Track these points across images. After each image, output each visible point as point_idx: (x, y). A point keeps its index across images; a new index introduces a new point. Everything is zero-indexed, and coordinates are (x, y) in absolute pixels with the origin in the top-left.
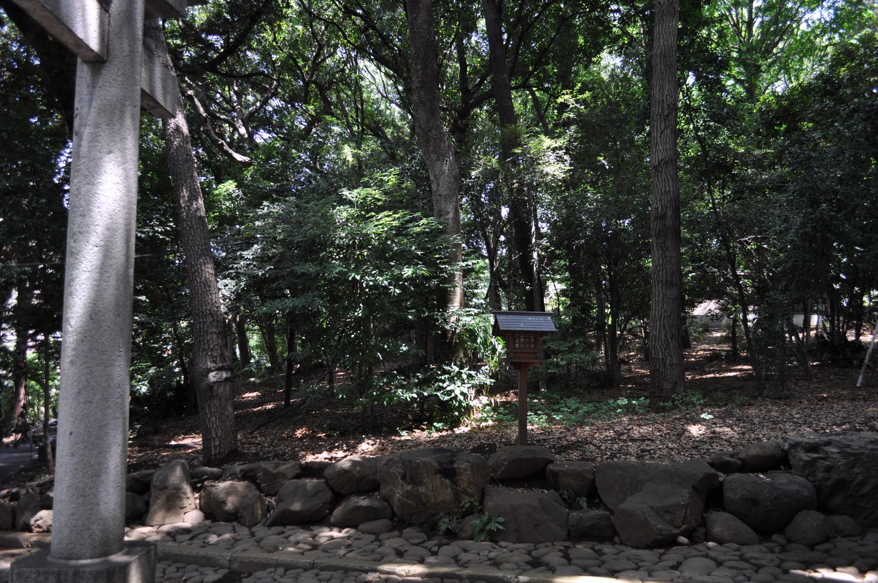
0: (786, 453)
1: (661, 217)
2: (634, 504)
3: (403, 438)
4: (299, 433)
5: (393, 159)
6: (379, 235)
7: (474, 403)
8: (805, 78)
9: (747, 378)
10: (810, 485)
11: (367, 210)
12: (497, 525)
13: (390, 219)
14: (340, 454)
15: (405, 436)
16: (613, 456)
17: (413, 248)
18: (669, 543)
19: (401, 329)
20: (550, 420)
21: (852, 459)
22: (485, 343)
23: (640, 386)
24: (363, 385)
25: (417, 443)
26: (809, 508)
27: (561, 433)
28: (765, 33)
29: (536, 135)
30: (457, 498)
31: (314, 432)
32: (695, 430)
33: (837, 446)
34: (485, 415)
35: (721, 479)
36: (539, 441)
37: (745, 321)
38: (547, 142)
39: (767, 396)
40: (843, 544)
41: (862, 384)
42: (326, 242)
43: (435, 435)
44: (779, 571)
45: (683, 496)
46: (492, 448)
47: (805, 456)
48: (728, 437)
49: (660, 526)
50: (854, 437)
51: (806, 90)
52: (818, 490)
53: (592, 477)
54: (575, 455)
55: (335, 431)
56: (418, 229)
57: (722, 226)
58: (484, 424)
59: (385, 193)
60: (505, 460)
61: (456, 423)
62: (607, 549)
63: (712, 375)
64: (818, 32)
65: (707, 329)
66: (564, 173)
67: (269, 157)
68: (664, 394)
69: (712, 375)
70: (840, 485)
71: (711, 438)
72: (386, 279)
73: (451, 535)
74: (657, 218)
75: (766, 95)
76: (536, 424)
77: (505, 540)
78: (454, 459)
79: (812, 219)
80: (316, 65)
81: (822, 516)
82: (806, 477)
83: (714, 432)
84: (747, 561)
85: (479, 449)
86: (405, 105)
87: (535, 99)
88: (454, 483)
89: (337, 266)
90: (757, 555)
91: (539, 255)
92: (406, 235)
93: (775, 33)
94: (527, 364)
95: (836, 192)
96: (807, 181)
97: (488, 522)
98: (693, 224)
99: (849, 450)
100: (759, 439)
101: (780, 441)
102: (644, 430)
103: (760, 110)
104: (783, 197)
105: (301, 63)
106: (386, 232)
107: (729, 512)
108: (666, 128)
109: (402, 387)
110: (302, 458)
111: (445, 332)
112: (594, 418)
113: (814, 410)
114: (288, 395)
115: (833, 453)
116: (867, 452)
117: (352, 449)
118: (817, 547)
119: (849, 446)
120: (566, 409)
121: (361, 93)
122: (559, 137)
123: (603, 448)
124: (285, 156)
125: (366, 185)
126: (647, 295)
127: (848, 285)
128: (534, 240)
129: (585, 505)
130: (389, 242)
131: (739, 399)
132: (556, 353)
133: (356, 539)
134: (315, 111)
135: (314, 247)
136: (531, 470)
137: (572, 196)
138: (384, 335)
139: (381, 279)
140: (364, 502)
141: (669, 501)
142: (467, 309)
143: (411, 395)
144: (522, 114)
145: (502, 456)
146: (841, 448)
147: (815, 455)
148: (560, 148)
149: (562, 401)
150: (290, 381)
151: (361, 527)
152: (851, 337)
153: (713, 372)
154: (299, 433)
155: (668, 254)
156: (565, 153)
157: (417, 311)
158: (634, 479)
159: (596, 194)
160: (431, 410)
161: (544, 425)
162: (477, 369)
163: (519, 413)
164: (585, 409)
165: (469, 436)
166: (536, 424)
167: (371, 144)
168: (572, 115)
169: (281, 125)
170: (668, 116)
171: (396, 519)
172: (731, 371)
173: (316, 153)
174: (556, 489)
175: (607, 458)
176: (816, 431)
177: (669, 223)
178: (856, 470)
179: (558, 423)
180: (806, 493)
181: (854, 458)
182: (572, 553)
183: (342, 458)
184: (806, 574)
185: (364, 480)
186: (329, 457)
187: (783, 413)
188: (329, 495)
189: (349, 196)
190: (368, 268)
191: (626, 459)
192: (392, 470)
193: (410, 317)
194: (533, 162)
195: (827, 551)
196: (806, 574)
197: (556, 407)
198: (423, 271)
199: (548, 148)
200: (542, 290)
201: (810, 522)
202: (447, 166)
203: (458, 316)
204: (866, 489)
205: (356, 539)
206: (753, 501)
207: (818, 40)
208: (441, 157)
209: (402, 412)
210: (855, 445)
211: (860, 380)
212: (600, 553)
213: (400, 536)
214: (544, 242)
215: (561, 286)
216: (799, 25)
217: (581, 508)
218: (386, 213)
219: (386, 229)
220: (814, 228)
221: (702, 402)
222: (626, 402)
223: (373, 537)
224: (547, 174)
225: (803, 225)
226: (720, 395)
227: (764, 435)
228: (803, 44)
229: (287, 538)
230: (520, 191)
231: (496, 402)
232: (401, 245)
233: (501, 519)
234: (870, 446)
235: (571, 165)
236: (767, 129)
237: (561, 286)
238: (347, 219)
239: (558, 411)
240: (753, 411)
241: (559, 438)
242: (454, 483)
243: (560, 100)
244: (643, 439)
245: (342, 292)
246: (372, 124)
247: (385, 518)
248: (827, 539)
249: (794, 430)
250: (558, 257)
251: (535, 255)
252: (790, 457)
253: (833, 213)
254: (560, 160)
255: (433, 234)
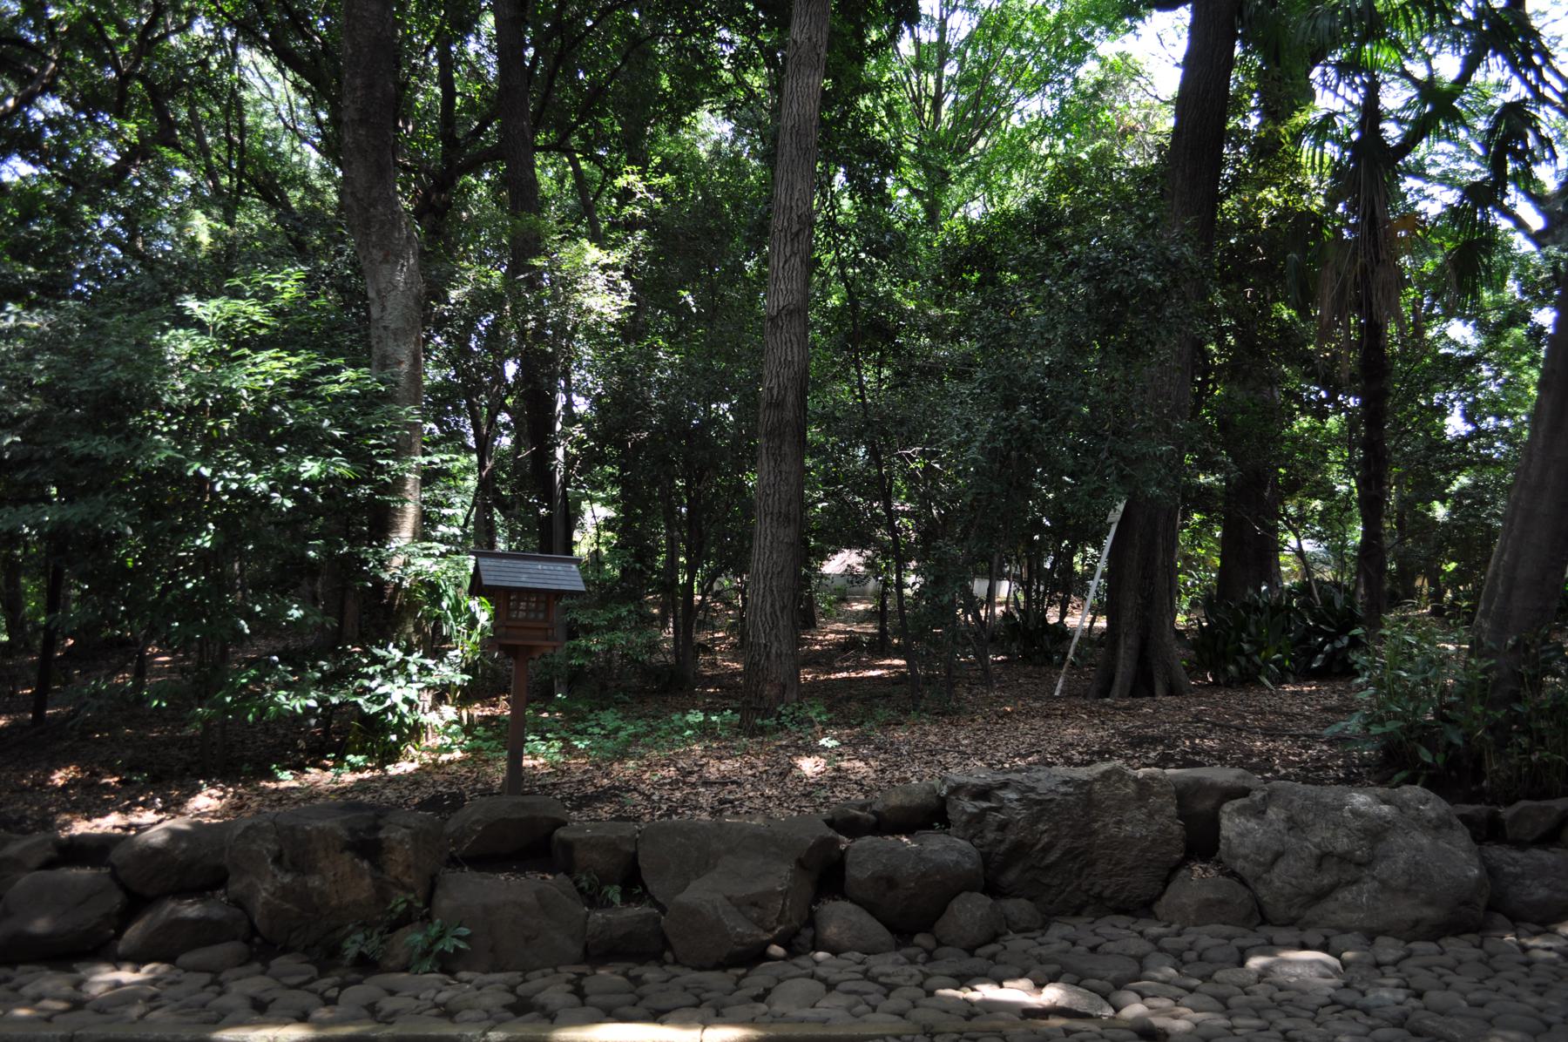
0: (943, 801)
1: (777, 405)
2: (702, 893)
3: (282, 785)
4: (58, 778)
5: (299, 250)
6: (255, 392)
7: (430, 718)
8: (1013, 202)
9: (899, 679)
10: (974, 852)
11: (236, 342)
12: (455, 942)
13: (281, 365)
14: (149, 817)
15: (287, 779)
16: (671, 811)
17: (326, 423)
18: (755, 956)
19: (291, 576)
20: (568, 749)
21: (1036, 808)
22: (455, 607)
23: (730, 691)
24: (205, 680)
25: (311, 794)
26: (970, 887)
27: (585, 772)
28: (959, 120)
29: (573, 237)
30: (381, 896)
31: (93, 774)
32: (809, 766)
33: (1017, 790)
34: (449, 741)
35: (843, 847)
36: (544, 786)
37: (901, 585)
38: (593, 253)
39: (925, 710)
40: (1017, 942)
41: (1062, 691)
42: (142, 397)
43: (349, 778)
44: (921, 992)
45: (779, 877)
46: (457, 801)
47: (970, 807)
48: (859, 776)
49: (742, 929)
50: (1041, 775)
51: (1010, 222)
52: (986, 858)
53: (632, 849)
54: (606, 811)
55: (140, 770)
56: (336, 389)
57: (877, 428)
58: (445, 757)
59: (277, 313)
60: (477, 822)
61: (393, 755)
62: (651, 973)
63: (845, 675)
64: (1035, 131)
65: (843, 599)
66: (620, 312)
67: (28, 215)
68: (761, 708)
69: (845, 675)
70: (1019, 850)
71: (833, 779)
72: (266, 479)
73: (367, 965)
74: (769, 405)
75: (953, 224)
76: (539, 756)
77: (468, 969)
78: (381, 822)
79: (1005, 428)
80: (147, 44)
81: (990, 901)
82: (971, 840)
83: (838, 769)
84: (874, 980)
85: (433, 803)
86: (329, 149)
87: (578, 172)
88: (377, 866)
89: (163, 448)
90: (889, 969)
91: (566, 454)
92: (313, 398)
93: (975, 123)
94: (531, 649)
95: (1042, 389)
96: (1001, 366)
97: (441, 936)
98: (828, 420)
99: (1032, 795)
100: (905, 780)
101: (936, 782)
102: (727, 766)
103: (943, 243)
104: (965, 389)
105: (113, 35)
106: (272, 388)
107: (853, 901)
108: (793, 254)
109: (288, 686)
110: (61, 827)
111: (380, 584)
112: (645, 746)
113: (990, 733)
114: (39, 702)
115: (1010, 800)
116: (1058, 798)
117: (173, 806)
118: (979, 951)
119: (1033, 789)
120: (597, 730)
121: (241, 115)
122: (613, 248)
123: (655, 798)
124: (66, 216)
125: (236, 294)
126: (747, 536)
127: (1057, 533)
128: (558, 427)
129: (617, 899)
130: (276, 409)
131: (882, 714)
132: (588, 630)
133: (171, 983)
134: (139, 134)
135: (119, 405)
136: (525, 837)
137: (631, 353)
138: (260, 586)
139: (254, 477)
140: (191, 910)
141: (758, 887)
142: (426, 544)
143: (304, 702)
144: (554, 197)
145: (473, 813)
146: (1022, 792)
147: (985, 805)
148: (615, 267)
149: (592, 716)
150: (46, 673)
151: (184, 959)
152: (1053, 617)
153: (847, 669)
154: (58, 778)
155: (784, 467)
156: (624, 277)
157: (327, 543)
158: (702, 850)
159: (672, 354)
160: (344, 730)
161: (556, 757)
162: (438, 654)
163: (510, 737)
164: (631, 729)
165: (413, 780)
166: (539, 756)
167: (255, 217)
168: (639, 212)
169: (63, 153)
170: (797, 234)
171: (257, 940)
172: (874, 668)
173: (137, 218)
174: (568, 873)
175: (661, 816)
176: (990, 765)
177: (789, 415)
178: (1042, 827)
179: (582, 754)
180: (968, 866)
181: (1040, 807)
182: (589, 984)
183: (152, 824)
184: (960, 994)
185: (195, 866)
186: (123, 823)
187: (945, 737)
188: (117, 899)
189: (199, 313)
190: (228, 455)
191: (692, 816)
192: (255, 847)
193: (312, 554)
194: (568, 284)
195: (992, 957)
196: (960, 994)
197: (579, 726)
198: (343, 468)
199: (594, 264)
200: (571, 518)
201: (971, 910)
202: (403, 275)
203: (407, 556)
204: (1052, 858)
205: (171, 983)
206: (889, 881)
207: (1035, 144)
208: (392, 256)
209: (285, 735)
210: (1041, 787)
211: (1060, 686)
212: (637, 981)
213: (263, 973)
214: (577, 431)
215: (604, 512)
216: (1008, 117)
217: (610, 904)
218: (271, 353)
219: (271, 383)
220: (1007, 442)
221: (824, 718)
222: (701, 717)
223: (206, 977)
224: (590, 311)
225: (992, 436)
226: (853, 708)
227: (914, 773)
228: (1012, 147)
229: (16, 989)
230: (538, 334)
231: (470, 717)
232: (301, 415)
233: (465, 931)
234: (1062, 789)
235: (632, 299)
236: (952, 275)
237: (604, 512)
238: (192, 358)
239: (581, 734)
240: (900, 734)
241: (581, 782)
242: (377, 866)
243: (620, 182)
244: (724, 782)
245: (170, 500)
246: (263, 177)
247: (235, 939)
248: (994, 938)
249: (959, 764)
250: (603, 460)
251: (560, 453)
252: (948, 808)
253: (1035, 421)
254: (613, 287)
255: (367, 401)
